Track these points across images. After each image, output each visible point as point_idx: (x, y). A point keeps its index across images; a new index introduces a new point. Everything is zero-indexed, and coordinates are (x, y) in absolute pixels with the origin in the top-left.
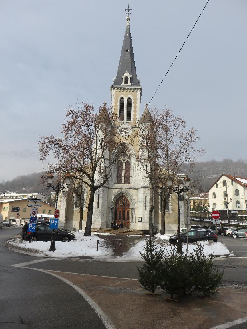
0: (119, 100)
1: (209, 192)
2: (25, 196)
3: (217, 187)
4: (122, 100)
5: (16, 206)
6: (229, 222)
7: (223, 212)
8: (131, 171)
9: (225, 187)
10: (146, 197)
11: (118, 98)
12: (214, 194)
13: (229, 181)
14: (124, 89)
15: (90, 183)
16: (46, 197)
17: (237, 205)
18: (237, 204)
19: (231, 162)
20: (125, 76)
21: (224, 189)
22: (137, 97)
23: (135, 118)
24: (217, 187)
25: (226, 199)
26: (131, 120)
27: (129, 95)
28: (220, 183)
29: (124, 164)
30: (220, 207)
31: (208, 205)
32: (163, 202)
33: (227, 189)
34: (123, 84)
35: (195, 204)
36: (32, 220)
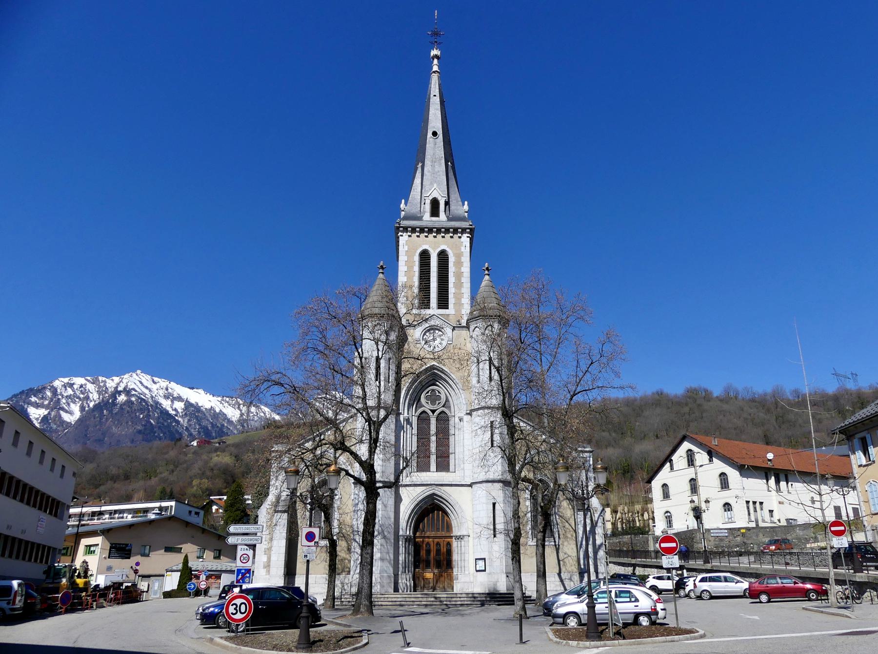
0: (417, 258)
1: (652, 482)
2: (146, 511)
3: (672, 468)
4: (425, 256)
5: (121, 540)
6: (298, 497)
7: (686, 537)
8: (451, 439)
9: (692, 469)
10: (494, 504)
11: (416, 252)
12: (665, 486)
13: (701, 457)
14: (430, 231)
15: (364, 477)
16: (197, 510)
17: (726, 513)
18: (725, 511)
19: (708, 396)
20: (431, 198)
21: (690, 473)
22: (463, 249)
23: (459, 304)
24: (672, 468)
25: (694, 502)
26: (448, 308)
27: (441, 245)
28: (679, 458)
29: (433, 421)
30: (684, 522)
31: (651, 516)
32: (540, 518)
33: (696, 474)
34: (427, 216)
35: (616, 518)
36: (240, 577)
